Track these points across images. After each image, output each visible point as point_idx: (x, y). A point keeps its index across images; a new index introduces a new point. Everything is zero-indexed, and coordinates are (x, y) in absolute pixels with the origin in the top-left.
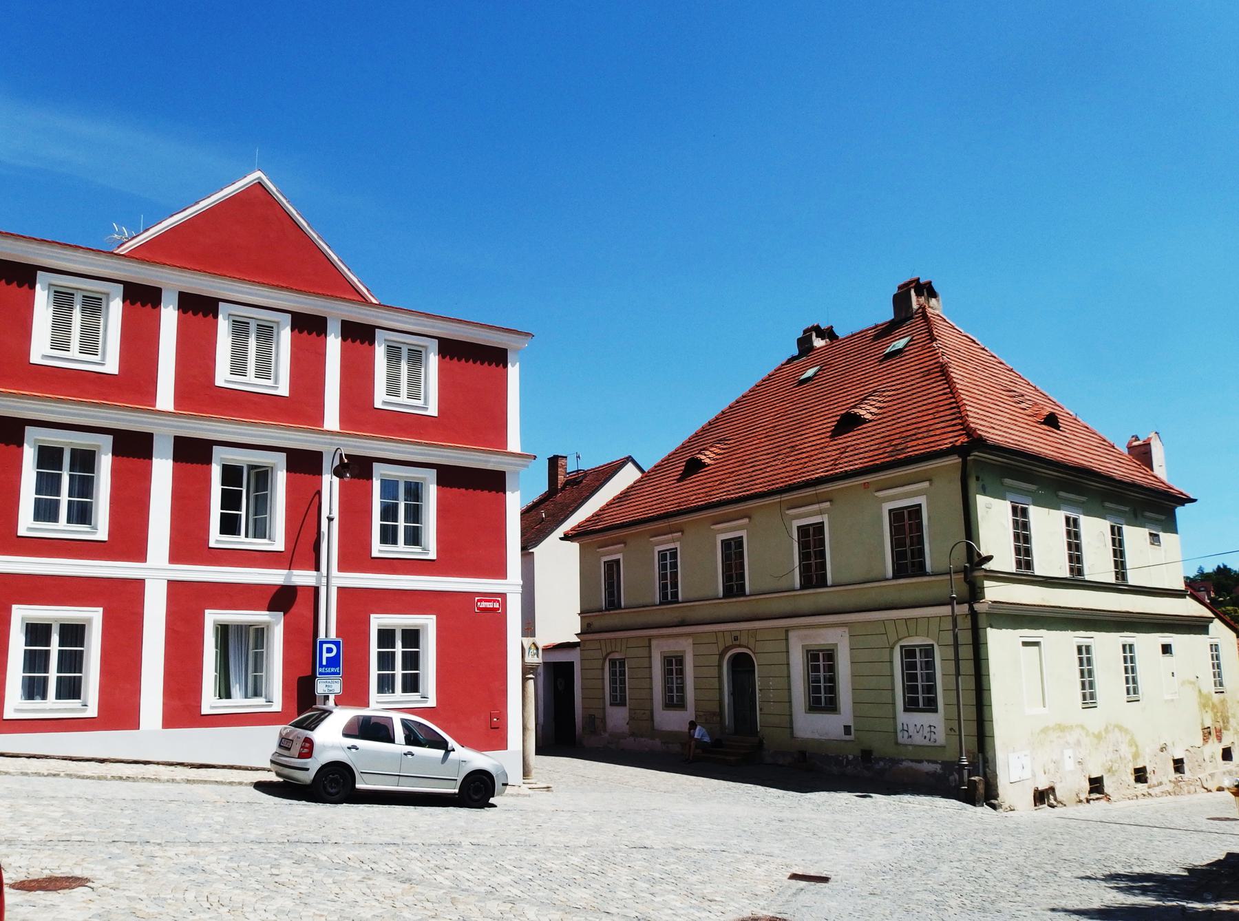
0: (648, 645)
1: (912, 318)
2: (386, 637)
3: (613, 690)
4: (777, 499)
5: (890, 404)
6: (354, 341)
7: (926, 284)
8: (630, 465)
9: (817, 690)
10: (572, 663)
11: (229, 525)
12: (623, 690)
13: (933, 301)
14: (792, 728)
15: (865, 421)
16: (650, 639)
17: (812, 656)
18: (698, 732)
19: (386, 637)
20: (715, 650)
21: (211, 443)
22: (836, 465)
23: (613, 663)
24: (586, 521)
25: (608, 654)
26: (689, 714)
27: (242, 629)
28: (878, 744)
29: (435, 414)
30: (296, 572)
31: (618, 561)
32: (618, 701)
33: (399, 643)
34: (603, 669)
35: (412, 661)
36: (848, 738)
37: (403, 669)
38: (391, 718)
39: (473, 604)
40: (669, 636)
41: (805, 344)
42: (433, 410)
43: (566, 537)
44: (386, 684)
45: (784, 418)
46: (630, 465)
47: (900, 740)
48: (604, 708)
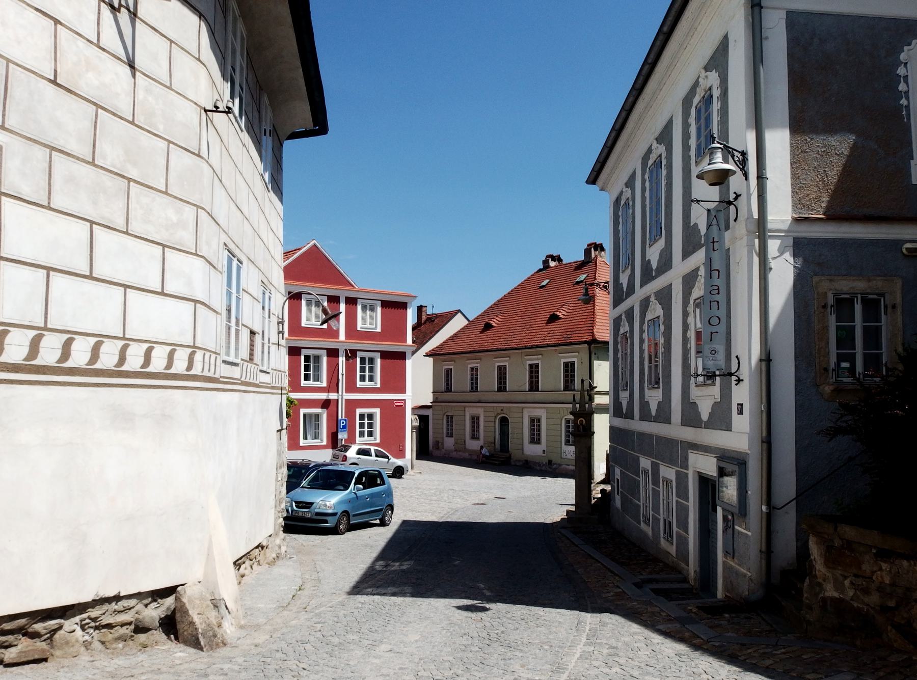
0: (463, 414)
1: (591, 262)
2: (362, 417)
3: (448, 429)
4: (521, 351)
5: (572, 311)
6: (350, 305)
7: (599, 245)
8: (459, 314)
9: (533, 434)
10: (428, 416)
11: (307, 378)
12: (452, 430)
13: (603, 253)
14: (523, 450)
15: (560, 318)
16: (465, 407)
17: (532, 420)
18: (484, 451)
19: (362, 417)
20: (493, 414)
21: (300, 348)
22: (545, 340)
23: (448, 417)
24: (436, 348)
25: (445, 413)
26: (481, 442)
27: (310, 415)
28: (555, 459)
29: (380, 331)
30: (330, 394)
31: (451, 369)
32: (450, 434)
33: (366, 419)
34: (443, 419)
35: (370, 425)
36: (544, 455)
37: (360, 420)
38: (370, 449)
39: (394, 404)
40: (476, 407)
41: (546, 262)
42: (379, 330)
43: (427, 355)
44: (362, 434)
45: (530, 307)
46: (459, 314)
47: (563, 456)
48: (443, 438)
